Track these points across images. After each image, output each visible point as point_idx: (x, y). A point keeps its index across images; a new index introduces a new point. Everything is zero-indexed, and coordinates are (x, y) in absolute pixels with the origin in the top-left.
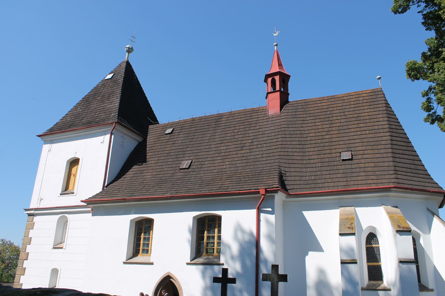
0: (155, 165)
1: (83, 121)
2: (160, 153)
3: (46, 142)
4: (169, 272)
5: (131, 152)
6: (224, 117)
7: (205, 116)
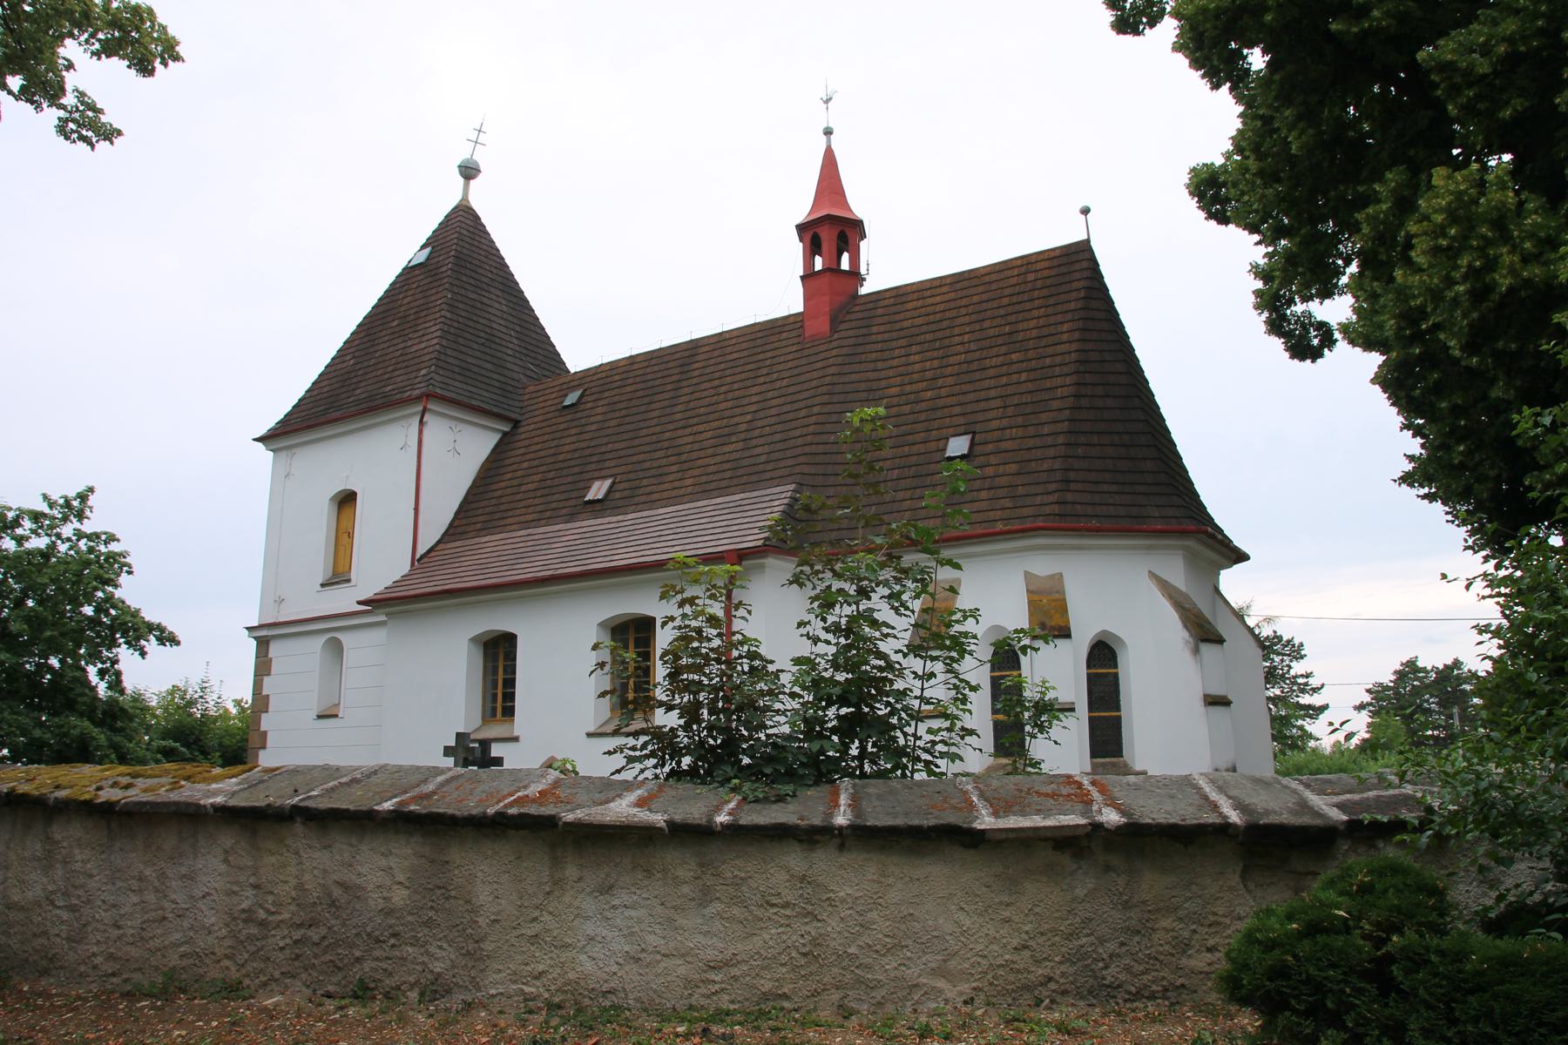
1: (358, 392)
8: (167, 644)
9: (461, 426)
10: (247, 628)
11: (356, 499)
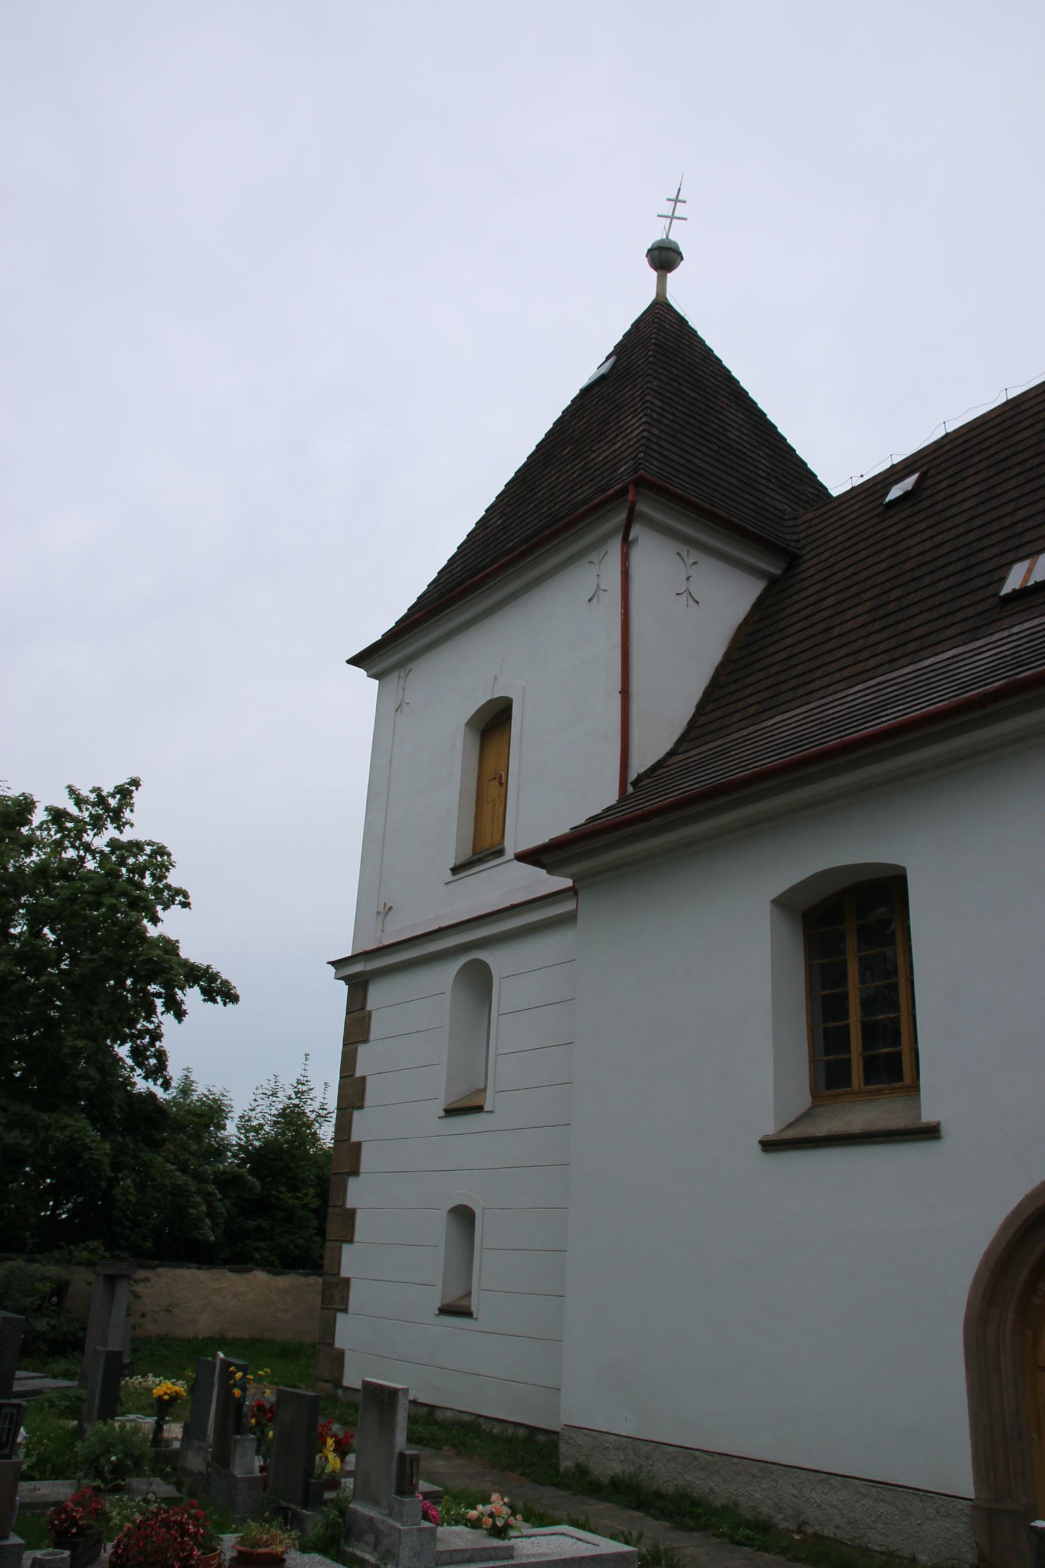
8: (219, 999)
9: (695, 555)
10: (333, 963)
11: (510, 718)
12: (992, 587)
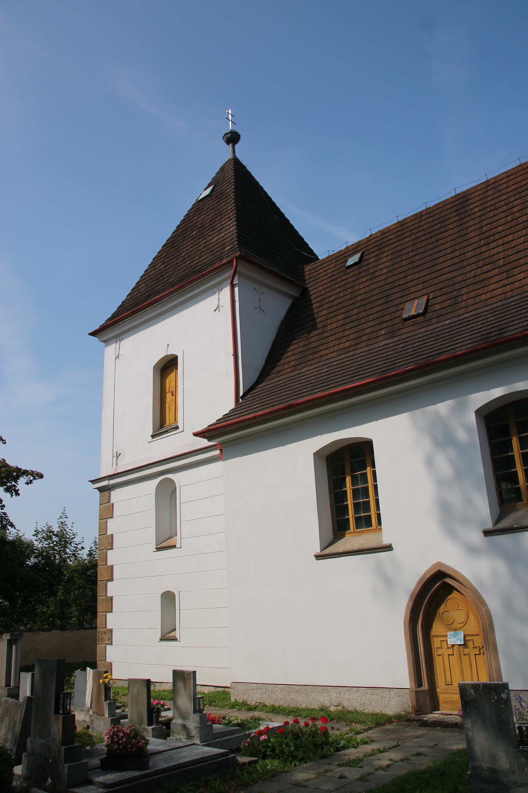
0: (341, 329)
2: (346, 303)
3: (107, 342)
4: (439, 564)
5: (281, 321)
6: (473, 195)
7: (427, 209)
11: (177, 363)
12: (398, 312)
